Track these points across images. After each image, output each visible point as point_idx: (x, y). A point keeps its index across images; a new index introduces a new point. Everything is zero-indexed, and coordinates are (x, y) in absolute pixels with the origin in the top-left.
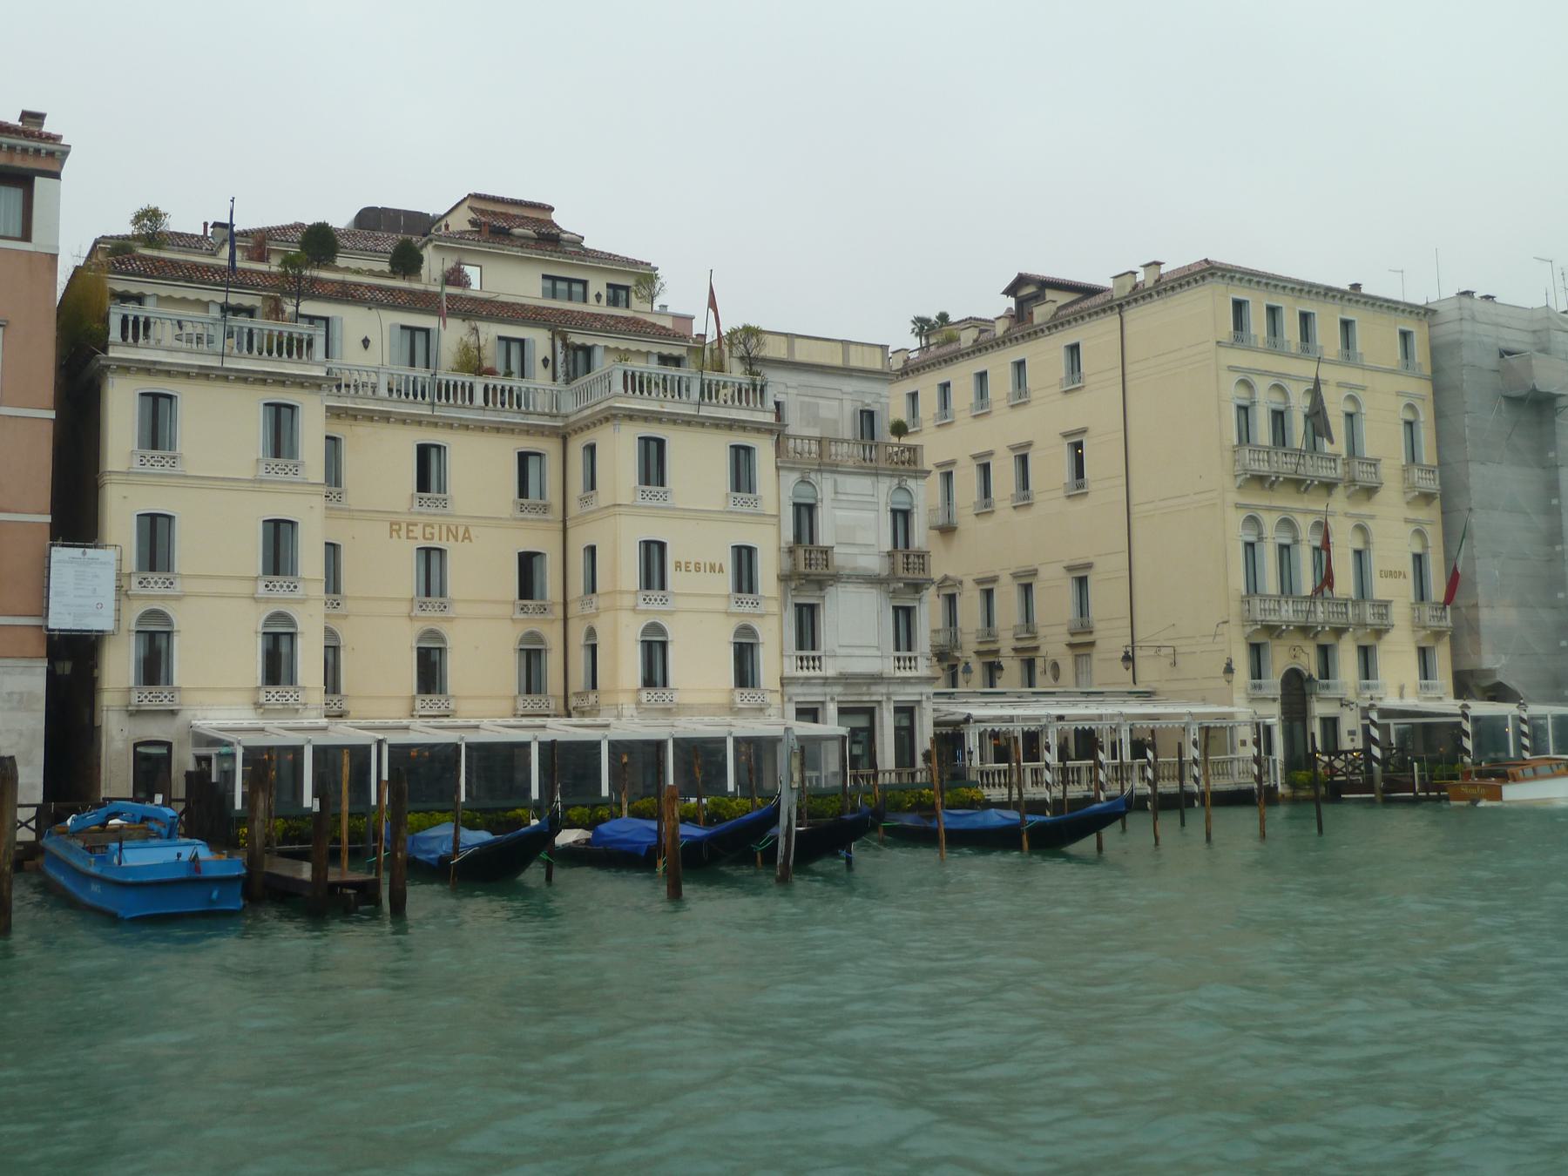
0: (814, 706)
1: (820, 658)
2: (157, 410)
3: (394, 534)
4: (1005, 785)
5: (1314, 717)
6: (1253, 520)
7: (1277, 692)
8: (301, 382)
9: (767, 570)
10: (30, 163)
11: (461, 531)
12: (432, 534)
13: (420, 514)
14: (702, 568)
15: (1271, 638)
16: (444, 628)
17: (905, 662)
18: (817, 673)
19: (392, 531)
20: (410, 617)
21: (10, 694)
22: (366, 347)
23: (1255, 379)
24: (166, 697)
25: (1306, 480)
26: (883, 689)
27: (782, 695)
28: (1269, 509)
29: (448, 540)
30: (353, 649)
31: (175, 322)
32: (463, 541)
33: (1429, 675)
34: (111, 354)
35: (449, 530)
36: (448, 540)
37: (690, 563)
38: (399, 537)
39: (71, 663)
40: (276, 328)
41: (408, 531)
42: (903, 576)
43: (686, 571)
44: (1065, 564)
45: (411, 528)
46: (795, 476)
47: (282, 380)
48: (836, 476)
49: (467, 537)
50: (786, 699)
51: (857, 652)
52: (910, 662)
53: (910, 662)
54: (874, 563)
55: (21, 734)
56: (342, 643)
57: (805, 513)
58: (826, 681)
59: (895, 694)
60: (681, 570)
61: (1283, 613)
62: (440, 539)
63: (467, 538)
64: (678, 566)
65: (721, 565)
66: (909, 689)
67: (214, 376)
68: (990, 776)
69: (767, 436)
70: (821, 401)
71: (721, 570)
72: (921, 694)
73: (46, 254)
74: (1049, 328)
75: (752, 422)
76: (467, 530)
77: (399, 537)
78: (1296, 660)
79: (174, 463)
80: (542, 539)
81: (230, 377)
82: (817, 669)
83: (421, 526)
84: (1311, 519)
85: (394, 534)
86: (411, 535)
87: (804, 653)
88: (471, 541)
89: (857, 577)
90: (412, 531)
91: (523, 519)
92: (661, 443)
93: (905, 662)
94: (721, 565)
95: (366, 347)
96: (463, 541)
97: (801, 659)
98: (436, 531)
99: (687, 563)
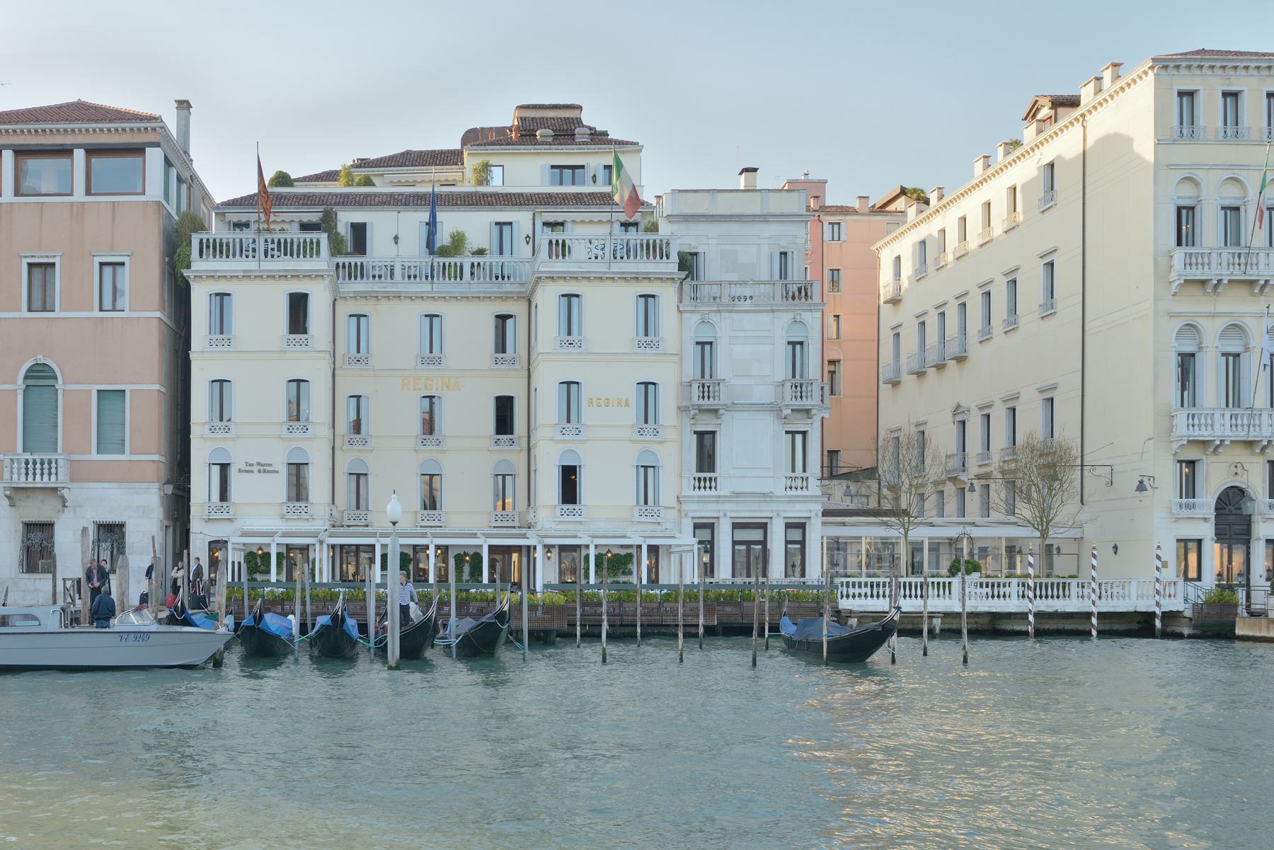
0: (711, 521)
1: (716, 479)
4: (922, 596)
5: (1259, 539)
6: (1191, 328)
7: (1211, 513)
8: (308, 276)
9: (667, 401)
10: (138, 139)
15: (1205, 454)
17: (705, 482)
18: (713, 492)
20: (415, 450)
22: (396, 243)
23: (1200, 175)
25: (1258, 280)
26: (774, 507)
27: (680, 511)
28: (1212, 315)
31: (588, 241)
33: (1196, 494)
42: (791, 403)
44: (1037, 386)
46: (696, 318)
47: (296, 276)
48: (734, 315)
50: (683, 514)
52: (710, 483)
53: (710, 483)
54: (764, 394)
58: (718, 499)
59: (784, 511)
61: (1217, 426)
65: (627, 399)
66: (798, 506)
69: (669, 284)
71: (627, 405)
72: (719, 511)
74: (1032, 149)
75: (655, 273)
78: (1238, 478)
80: (512, 386)
84: (1221, 323)
87: (702, 475)
89: (431, 412)
91: (498, 370)
93: (705, 482)
94: (627, 399)
95: (396, 243)
97: (699, 479)
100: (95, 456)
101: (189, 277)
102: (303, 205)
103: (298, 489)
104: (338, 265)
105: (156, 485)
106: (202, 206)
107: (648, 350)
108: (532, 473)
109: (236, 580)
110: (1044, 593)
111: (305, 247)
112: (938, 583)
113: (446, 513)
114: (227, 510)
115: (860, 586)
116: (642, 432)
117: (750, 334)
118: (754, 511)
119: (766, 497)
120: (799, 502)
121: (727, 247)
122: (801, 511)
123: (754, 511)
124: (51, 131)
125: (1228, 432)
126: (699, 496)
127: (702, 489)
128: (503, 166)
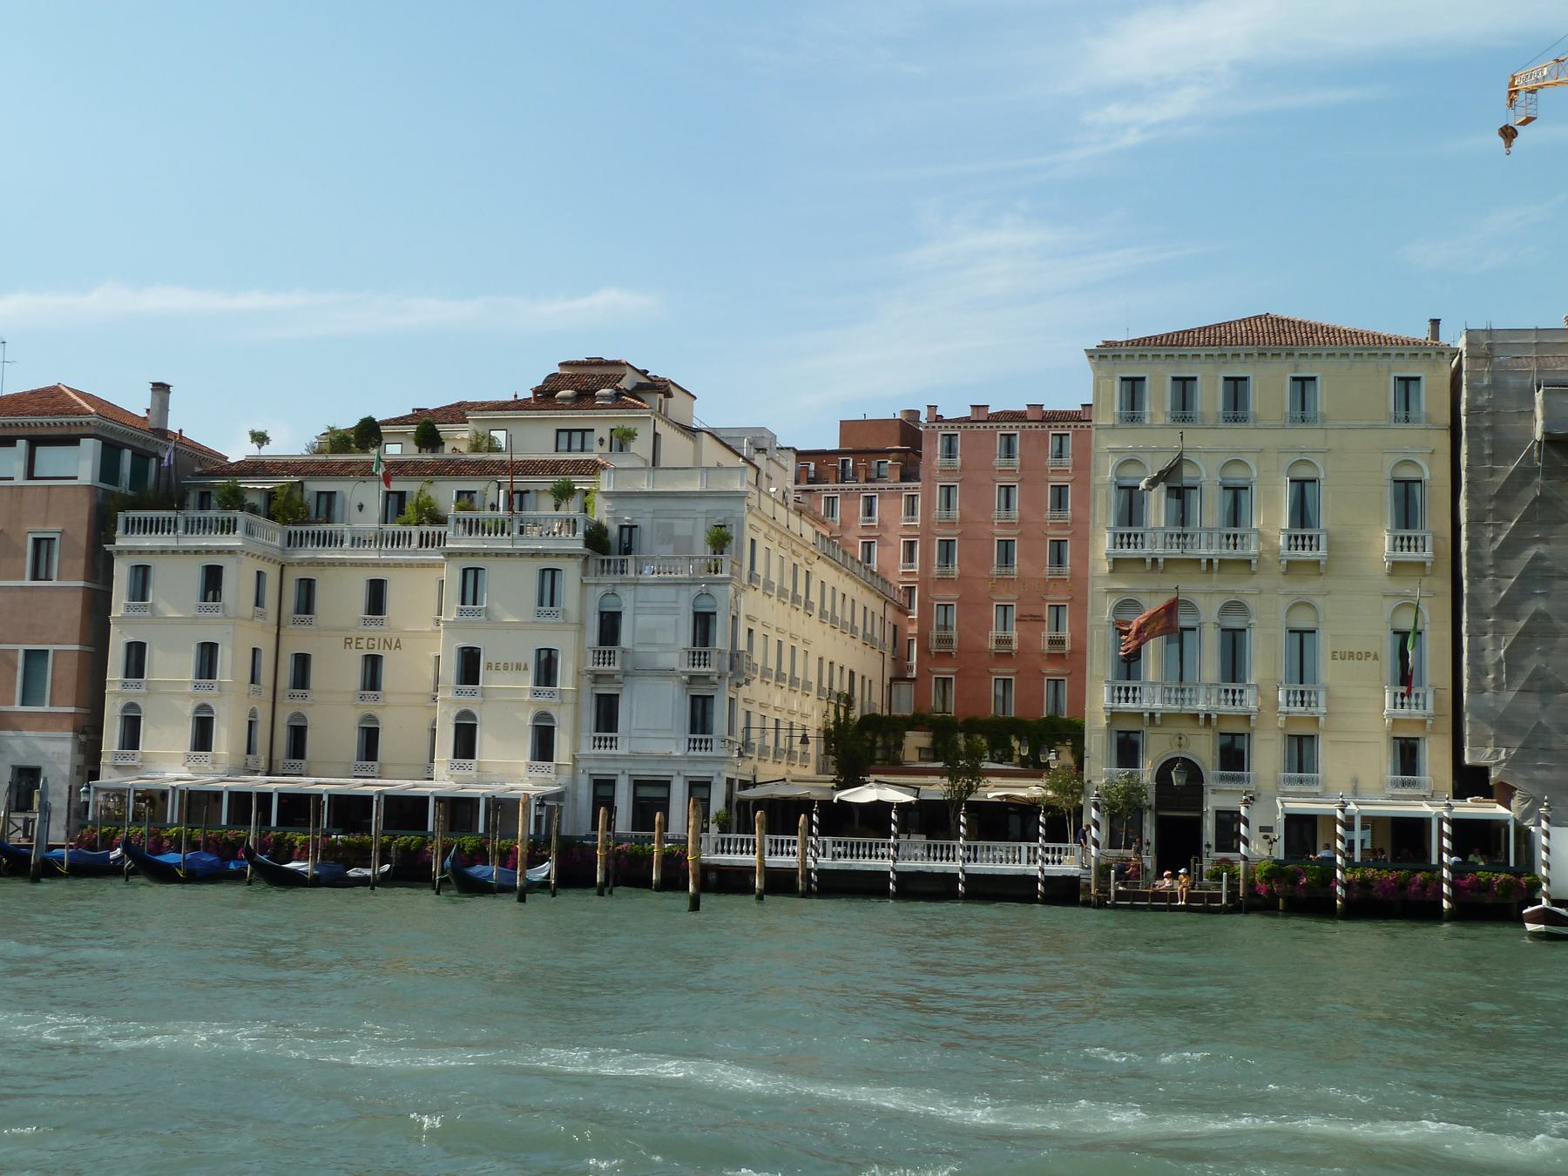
2: (141, 577)
3: (348, 645)
10: (74, 431)
12: (373, 645)
13: (365, 630)
14: (510, 668)
16: (378, 713)
18: (613, 751)
19: (346, 643)
22: (360, 510)
29: (384, 648)
34: (117, 544)
35: (385, 641)
36: (384, 648)
38: (351, 648)
39: (908, 733)
41: (357, 643)
56: (309, 723)
57: (610, 626)
58: (615, 758)
62: (379, 648)
65: (526, 665)
68: (726, 842)
70: (676, 522)
71: (526, 669)
72: (712, 771)
76: (398, 640)
77: (351, 648)
84: (1218, 602)
85: (348, 645)
86: (359, 646)
92: (146, 569)
93: (611, 742)
94: (526, 665)
95: (360, 510)
98: (376, 642)
100: (18, 708)
102: (579, 474)
103: (203, 738)
105: (71, 734)
107: (548, 619)
110: (855, 852)
112: (871, 844)
113: (381, 764)
115: (1054, 852)
116: (460, 693)
117: (656, 605)
119: (667, 759)
120: (702, 762)
121: (662, 521)
122: (705, 771)
123: (653, 770)
124: (35, 424)
125: (1158, 705)
126: (595, 755)
127: (602, 748)
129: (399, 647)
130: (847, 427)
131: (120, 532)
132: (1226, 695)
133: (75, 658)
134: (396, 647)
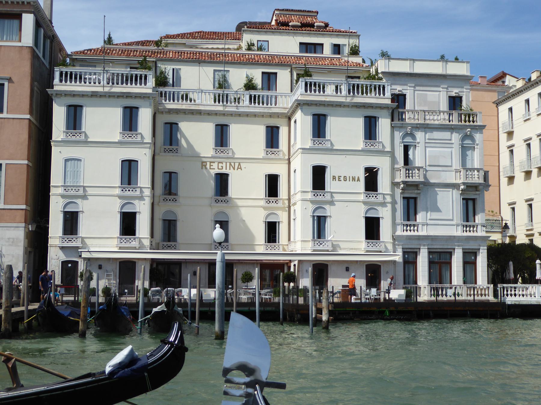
0: (415, 250)
3: (204, 167)
11: (237, 165)
12: (222, 167)
21: (9, 239)
24: (66, 241)
29: (230, 169)
30: (183, 221)
32: (237, 170)
34: (54, 89)
35: (230, 164)
36: (230, 169)
37: (341, 177)
40: (368, 83)
41: (210, 166)
43: (339, 180)
45: (212, 164)
49: (240, 168)
51: (112, 246)
55: (13, 256)
60: (335, 180)
62: (226, 169)
63: (239, 168)
64: (334, 178)
65: (358, 178)
67: (125, 96)
71: (358, 180)
73: (27, 47)
76: (239, 164)
79: (81, 135)
81: (62, 94)
82: (416, 231)
83: (216, 163)
85: (204, 167)
86: (212, 167)
88: (241, 170)
90: (212, 166)
94: (358, 178)
96: (237, 170)
99: (339, 177)
101: (52, 94)
104: (161, 93)
105: (23, 225)
106: (59, 55)
108: (292, 221)
109: (415, 301)
111: (118, 80)
114: (278, 248)
118: (443, 245)
128: (268, 41)
129: (241, 168)
130: (166, 35)
131: (56, 80)
132: (473, 229)
133: (25, 168)
134: (238, 168)
